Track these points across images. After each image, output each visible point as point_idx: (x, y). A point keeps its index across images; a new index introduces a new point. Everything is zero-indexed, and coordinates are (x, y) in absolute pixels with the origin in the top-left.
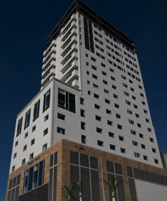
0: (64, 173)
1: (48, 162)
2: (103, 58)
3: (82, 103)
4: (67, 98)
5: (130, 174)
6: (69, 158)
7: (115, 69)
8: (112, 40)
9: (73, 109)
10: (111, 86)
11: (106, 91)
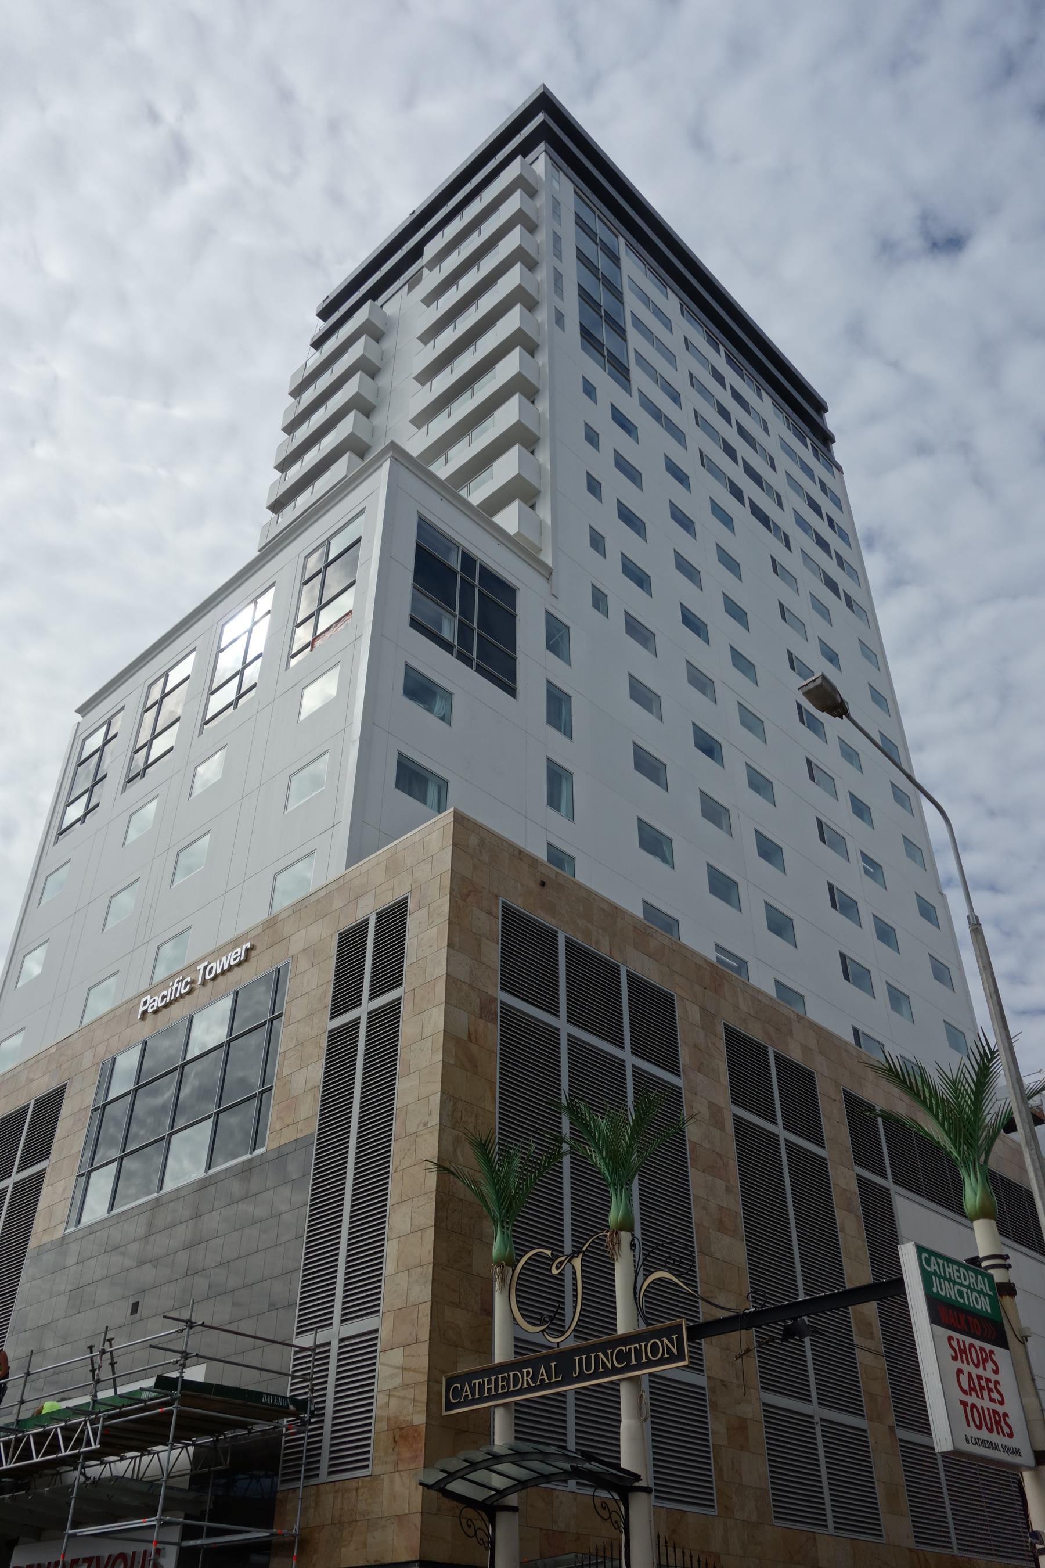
0: (459, 1049)
1: (313, 982)
2: (678, 435)
3: (554, 801)
4: (467, 588)
5: (864, 1152)
6: (494, 954)
7: (740, 514)
8: (720, 362)
9: (498, 665)
11: (700, 682)
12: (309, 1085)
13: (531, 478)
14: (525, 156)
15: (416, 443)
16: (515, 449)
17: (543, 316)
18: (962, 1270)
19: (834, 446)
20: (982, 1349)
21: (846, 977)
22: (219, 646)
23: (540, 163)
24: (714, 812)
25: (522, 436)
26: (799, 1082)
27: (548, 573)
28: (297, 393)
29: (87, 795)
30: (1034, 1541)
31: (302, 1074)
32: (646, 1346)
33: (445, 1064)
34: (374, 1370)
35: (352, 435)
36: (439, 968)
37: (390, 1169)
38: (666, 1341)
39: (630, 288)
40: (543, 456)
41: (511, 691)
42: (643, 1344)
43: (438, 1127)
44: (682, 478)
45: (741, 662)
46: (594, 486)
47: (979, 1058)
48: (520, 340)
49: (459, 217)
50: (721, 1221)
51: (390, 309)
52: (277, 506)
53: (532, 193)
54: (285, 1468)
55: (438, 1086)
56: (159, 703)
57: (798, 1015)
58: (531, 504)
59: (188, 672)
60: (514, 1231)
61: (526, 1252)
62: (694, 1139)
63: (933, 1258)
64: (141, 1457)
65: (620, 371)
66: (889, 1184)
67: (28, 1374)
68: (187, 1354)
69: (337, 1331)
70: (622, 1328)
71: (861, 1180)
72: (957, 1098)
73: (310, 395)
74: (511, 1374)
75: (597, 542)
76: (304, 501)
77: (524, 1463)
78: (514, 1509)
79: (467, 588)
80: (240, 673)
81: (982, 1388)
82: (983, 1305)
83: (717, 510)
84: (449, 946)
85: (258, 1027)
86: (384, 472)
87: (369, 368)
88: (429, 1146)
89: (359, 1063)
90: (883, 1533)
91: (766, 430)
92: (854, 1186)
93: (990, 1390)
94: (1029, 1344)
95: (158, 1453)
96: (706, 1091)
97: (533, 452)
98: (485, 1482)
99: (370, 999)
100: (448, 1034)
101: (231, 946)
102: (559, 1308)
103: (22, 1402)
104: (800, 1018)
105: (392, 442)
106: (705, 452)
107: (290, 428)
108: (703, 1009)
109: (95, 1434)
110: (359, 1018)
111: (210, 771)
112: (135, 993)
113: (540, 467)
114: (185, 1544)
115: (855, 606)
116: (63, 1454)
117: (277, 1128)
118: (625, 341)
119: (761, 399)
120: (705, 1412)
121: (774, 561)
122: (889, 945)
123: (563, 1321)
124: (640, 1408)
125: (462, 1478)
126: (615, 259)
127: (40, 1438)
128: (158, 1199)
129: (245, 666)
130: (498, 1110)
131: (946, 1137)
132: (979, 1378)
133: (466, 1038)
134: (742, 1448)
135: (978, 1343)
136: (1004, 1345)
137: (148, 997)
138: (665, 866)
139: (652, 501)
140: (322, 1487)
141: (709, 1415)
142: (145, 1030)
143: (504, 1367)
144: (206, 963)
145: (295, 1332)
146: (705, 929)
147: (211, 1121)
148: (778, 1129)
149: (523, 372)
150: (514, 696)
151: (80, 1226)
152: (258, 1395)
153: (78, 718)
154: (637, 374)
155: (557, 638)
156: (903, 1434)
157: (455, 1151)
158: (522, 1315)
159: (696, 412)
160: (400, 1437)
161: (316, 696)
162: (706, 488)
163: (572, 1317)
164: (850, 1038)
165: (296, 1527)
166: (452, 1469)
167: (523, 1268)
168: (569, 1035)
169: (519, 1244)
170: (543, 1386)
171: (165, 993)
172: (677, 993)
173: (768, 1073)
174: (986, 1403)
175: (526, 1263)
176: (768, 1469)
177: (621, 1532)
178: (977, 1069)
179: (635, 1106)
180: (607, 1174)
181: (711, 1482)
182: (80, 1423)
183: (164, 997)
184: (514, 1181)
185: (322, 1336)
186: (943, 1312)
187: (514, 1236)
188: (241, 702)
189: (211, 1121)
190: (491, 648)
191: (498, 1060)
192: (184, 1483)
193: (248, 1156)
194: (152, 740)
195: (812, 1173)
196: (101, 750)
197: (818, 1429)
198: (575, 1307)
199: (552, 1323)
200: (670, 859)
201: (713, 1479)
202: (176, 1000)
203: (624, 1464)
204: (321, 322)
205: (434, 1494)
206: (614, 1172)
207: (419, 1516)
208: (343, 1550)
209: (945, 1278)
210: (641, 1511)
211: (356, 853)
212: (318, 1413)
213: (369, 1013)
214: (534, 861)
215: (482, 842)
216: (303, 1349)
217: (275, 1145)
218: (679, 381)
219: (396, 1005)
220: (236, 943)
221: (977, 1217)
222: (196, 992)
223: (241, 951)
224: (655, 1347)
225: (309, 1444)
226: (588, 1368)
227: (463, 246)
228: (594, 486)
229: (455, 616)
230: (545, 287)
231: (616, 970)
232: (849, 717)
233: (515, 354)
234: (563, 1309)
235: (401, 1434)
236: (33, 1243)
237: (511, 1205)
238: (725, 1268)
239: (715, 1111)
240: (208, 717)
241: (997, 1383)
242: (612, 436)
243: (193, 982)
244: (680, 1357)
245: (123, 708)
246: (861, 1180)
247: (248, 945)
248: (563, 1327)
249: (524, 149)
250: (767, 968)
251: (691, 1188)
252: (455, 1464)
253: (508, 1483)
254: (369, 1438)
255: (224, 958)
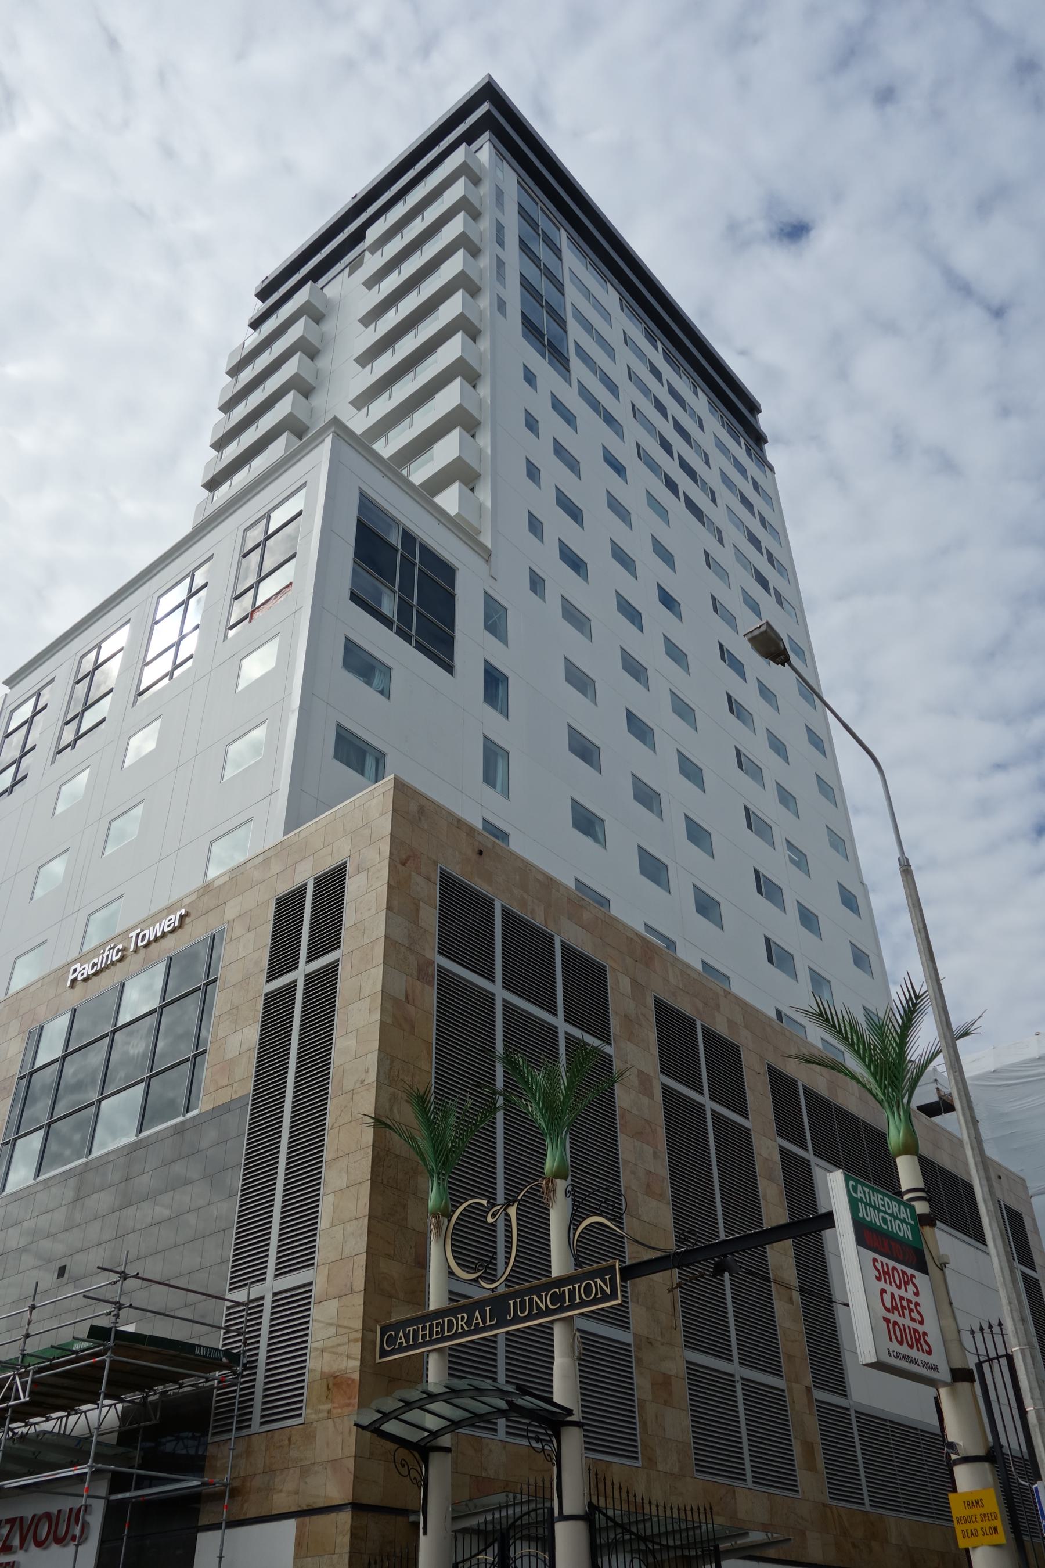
1: (247, 952)
3: (489, 778)
5: (787, 1124)
6: (431, 918)
7: (676, 507)
8: (657, 357)
9: (437, 642)
10: (611, 830)
11: (635, 669)
12: (245, 1048)
14: (469, 144)
15: (359, 423)
18: (886, 1199)
19: (767, 447)
20: (904, 1273)
21: (771, 960)
23: (485, 152)
25: (461, 419)
26: (725, 1056)
27: (487, 555)
28: (234, 371)
29: (26, 726)
30: (950, 1451)
31: (235, 1040)
32: (580, 1287)
33: (382, 1024)
35: (290, 415)
36: (379, 929)
37: (326, 1127)
38: (599, 1281)
39: (571, 280)
40: (484, 440)
41: (449, 669)
42: (577, 1286)
43: (375, 1084)
44: (619, 469)
46: (533, 472)
47: (904, 1002)
49: (402, 202)
51: (330, 292)
52: (212, 485)
54: (216, 1414)
55: (376, 1044)
56: (91, 674)
58: (471, 486)
60: (450, 1182)
61: (462, 1203)
62: (623, 1105)
63: (859, 1186)
64: (67, 1417)
66: (809, 1155)
68: (121, 1305)
69: (271, 1285)
70: (556, 1271)
71: (783, 1151)
72: (883, 1041)
73: (247, 375)
76: (241, 478)
77: (456, 1401)
78: (447, 1450)
80: (177, 645)
81: (903, 1308)
82: (905, 1232)
83: (653, 501)
84: (387, 908)
85: (193, 984)
87: (309, 349)
88: (367, 1103)
89: (297, 1026)
92: (777, 1157)
93: (911, 1311)
94: (947, 1271)
95: (85, 1412)
96: (635, 1056)
97: (473, 436)
98: (419, 1423)
99: (308, 962)
101: (165, 913)
104: (727, 993)
105: (335, 418)
106: (642, 445)
107: (227, 407)
108: (634, 981)
110: (296, 981)
111: (143, 743)
112: (64, 962)
113: (480, 451)
114: (113, 1497)
115: (784, 603)
117: (212, 1090)
120: (631, 1367)
121: (707, 554)
122: (811, 931)
123: (495, 1270)
124: (573, 1347)
125: (396, 1418)
126: (557, 252)
129: (182, 637)
130: (434, 1070)
131: (872, 1080)
132: (901, 1298)
133: (403, 999)
134: (666, 1403)
135: (900, 1267)
136: (924, 1270)
137: (78, 965)
138: (597, 846)
139: (591, 488)
141: (634, 1371)
142: (74, 998)
143: (439, 1314)
144: (138, 931)
145: (228, 1288)
146: (635, 906)
148: (705, 1099)
149: (466, 358)
150: (452, 673)
153: (6, 689)
154: (576, 364)
155: (495, 620)
158: (458, 1264)
160: (335, 1384)
161: (256, 666)
162: (641, 480)
163: (504, 1270)
164: (773, 1015)
165: (228, 1476)
166: (387, 1409)
167: (458, 1218)
168: (504, 1000)
170: (477, 1330)
171: (95, 960)
172: (609, 964)
173: (696, 1046)
174: (906, 1322)
175: (461, 1214)
176: (691, 1423)
177: (553, 1464)
178: (900, 1022)
180: (543, 1124)
181: (635, 1435)
182: (8, 1377)
183: (95, 964)
184: (451, 1135)
185: (256, 1291)
186: (868, 1236)
187: (450, 1188)
188: (177, 673)
191: (435, 1022)
192: (112, 1439)
193: (181, 1119)
195: (737, 1144)
196: (29, 722)
197: (739, 1387)
198: (507, 1264)
199: (485, 1272)
200: (602, 840)
201: (638, 1432)
202: (107, 967)
203: (556, 1399)
204: (260, 303)
205: (368, 1434)
206: (550, 1123)
207: (352, 1460)
208: (275, 1497)
209: (870, 1205)
210: (572, 1442)
211: (294, 819)
212: (251, 1366)
214: (471, 830)
216: (238, 1304)
217: (209, 1107)
219: (334, 967)
221: (900, 1154)
222: (127, 960)
223: (175, 918)
224: (588, 1288)
225: (241, 1396)
226: (523, 1311)
227: (406, 231)
228: (533, 472)
229: (394, 592)
231: (550, 939)
232: (790, 665)
233: (457, 339)
234: (495, 1264)
235: (334, 1383)
239: (644, 1079)
241: (917, 1304)
242: (552, 424)
243: (124, 949)
244: (613, 1296)
245: (53, 680)
246: (783, 1151)
247: (183, 912)
248: (495, 1276)
249: (469, 137)
250: (695, 944)
251: (620, 1152)
252: (390, 1404)
254: (303, 1387)
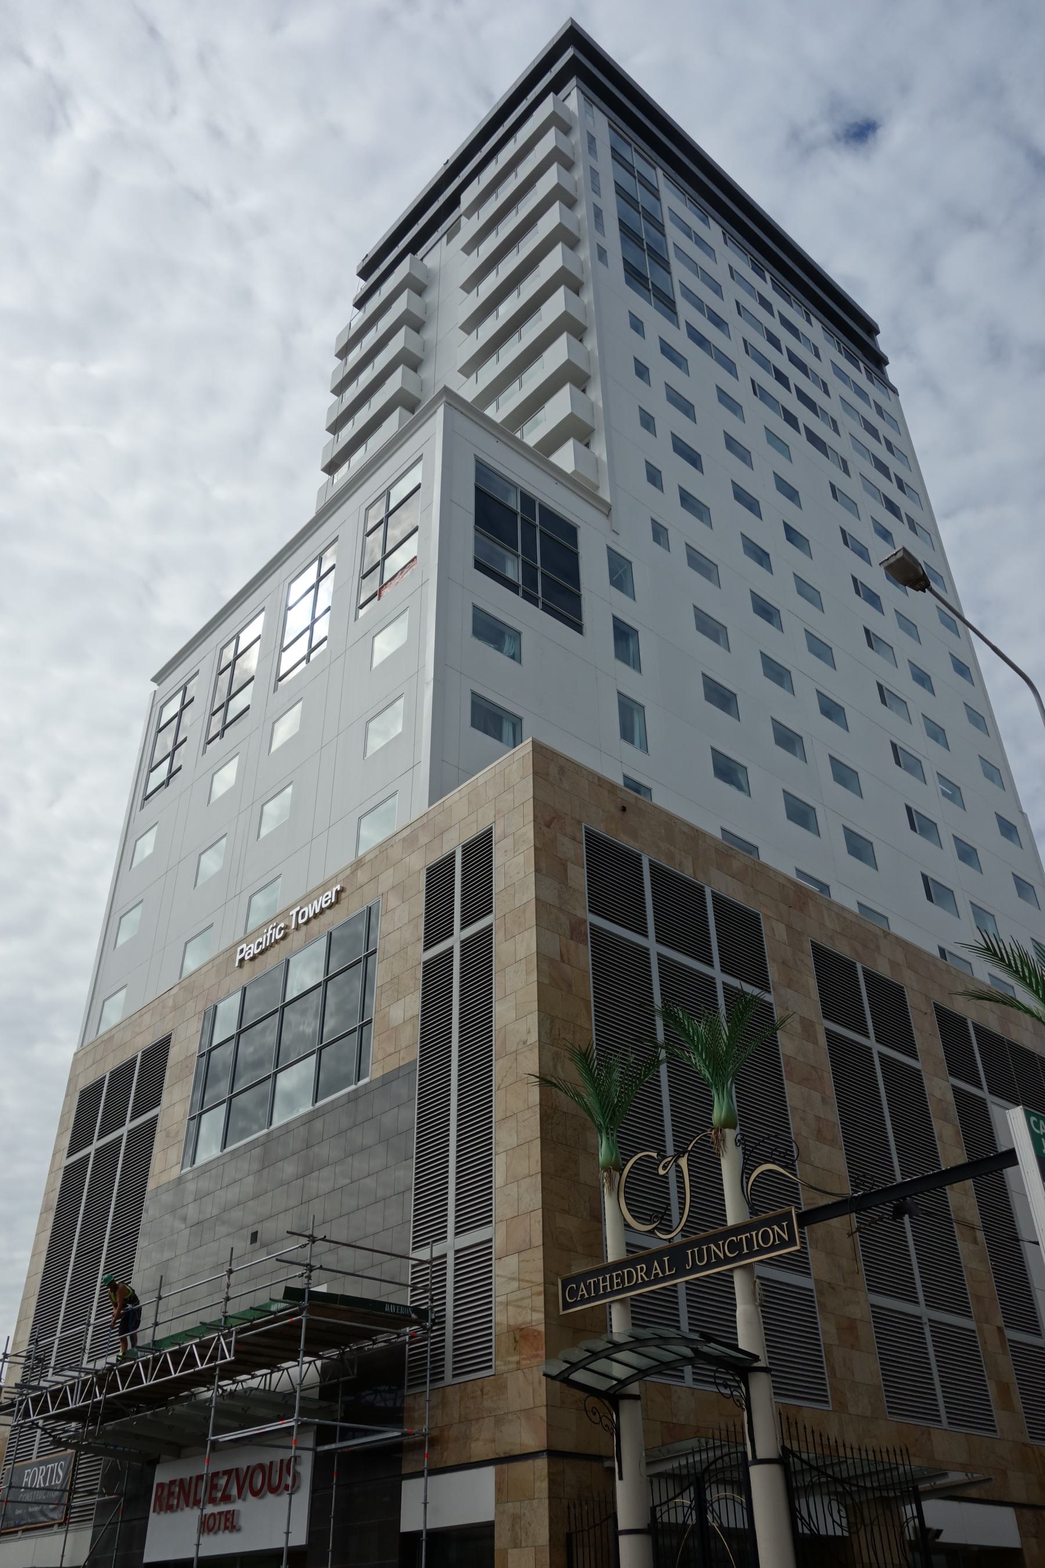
2: (730, 366)
3: (627, 734)
4: (529, 526)
5: (958, 1063)
6: (579, 877)
7: (797, 441)
8: (766, 289)
12: (408, 1015)
13: (584, 416)
14: (557, 93)
15: (469, 390)
16: (567, 389)
17: (585, 253)
19: (888, 369)
22: (287, 605)
24: (787, 739)
25: (572, 375)
26: (889, 997)
27: (606, 510)
28: (343, 354)
29: (169, 759)
31: (400, 1011)
32: (757, 1235)
33: (540, 984)
34: (491, 1284)
37: (493, 1088)
38: (776, 1228)
40: (595, 393)
41: (578, 628)
42: (754, 1233)
45: (805, 590)
48: (566, 279)
50: (819, 1131)
51: (431, 262)
53: (566, 130)
56: (232, 664)
57: (884, 931)
58: (586, 442)
59: (259, 632)
61: (632, 1157)
62: (788, 1053)
64: (271, 1374)
65: (667, 304)
66: (984, 1094)
67: (160, 1298)
68: (312, 1267)
69: (452, 1244)
70: (731, 1221)
71: (956, 1090)
73: (355, 355)
74: (625, 1271)
75: (654, 476)
76: (359, 458)
77: (641, 1350)
78: (636, 1398)
79: (529, 526)
83: (772, 438)
84: (536, 871)
85: (354, 958)
86: (437, 421)
87: (414, 322)
88: (531, 1063)
89: (458, 989)
90: (997, 1428)
91: (817, 355)
92: (950, 1097)
95: (287, 1369)
96: (795, 998)
97: (584, 391)
98: (606, 1372)
100: (541, 955)
102: (665, 1214)
103: (156, 1324)
104: (887, 934)
105: (445, 387)
108: (789, 927)
109: (228, 1344)
110: (452, 948)
113: (592, 405)
114: (320, 1449)
116: (200, 1368)
118: (670, 273)
119: (811, 324)
120: (815, 1318)
124: (754, 1293)
126: (655, 192)
127: (176, 1355)
128: (268, 1134)
129: (314, 620)
130: (594, 1027)
133: (558, 958)
134: (853, 1347)
137: (244, 946)
139: (706, 433)
140: (448, 1389)
142: (244, 976)
143: (618, 1265)
146: (784, 851)
147: (314, 1057)
150: (581, 633)
151: (195, 1166)
152: (381, 1305)
153: (154, 686)
154: (684, 308)
155: (620, 574)
156: (1011, 1334)
157: (555, 1067)
158: (633, 1216)
159: (745, 341)
160: (521, 1337)
164: (936, 953)
165: (426, 1426)
166: (574, 1360)
167: (630, 1172)
168: (659, 954)
169: (624, 1148)
170: (657, 1280)
171: (260, 940)
172: (762, 911)
173: (858, 988)
175: (632, 1167)
179: (727, 1022)
180: (708, 1075)
183: (260, 944)
184: (616, 1090)
185: (438, 1249)
187: (619, 1142)
188: (313, 656)
189: (314, 1057)
190: (557, 590)
192: (315, 1394)
193: (353, 1087)
194: (229, 700)
195: (907, 1085)
196: (179, 715)
197: (927, 1330)
198: (682, 1214)
200: (745, 788)
202: (271, 945)
204: (362, 282)
205: (558, 1384)
207: (544, 1409)
208: (473, 1445)
210: (760, 1388)
211: (438, 789)
212: (440, 1321)
213: (462, 942)
214: (612, 787)
215: (562, 771)
216: (422, 1262)
218: (725, 309)
219: (488, 931)
220: (325, 886)
222: (290, 937)
223: (331, 894)
226: (701, 1259)
229: (517, 556)
230: (586, 224)
231: (701, 891)
235: (521, 1335)
236: (151, 1185)
237: (614, 1113)
238: (825, 1165)
240: (281, 674)
242: (662, 369)
243: (286, 927)
244: (792, 1242)
245: (197, 673)
246: (956, 1090)
247: (338, 887)
248: (671, 1226)
249: (556, 86)
250: (849, 887)
252: (577, 1354)
253: (630, 1372)
255: (315, 902)
